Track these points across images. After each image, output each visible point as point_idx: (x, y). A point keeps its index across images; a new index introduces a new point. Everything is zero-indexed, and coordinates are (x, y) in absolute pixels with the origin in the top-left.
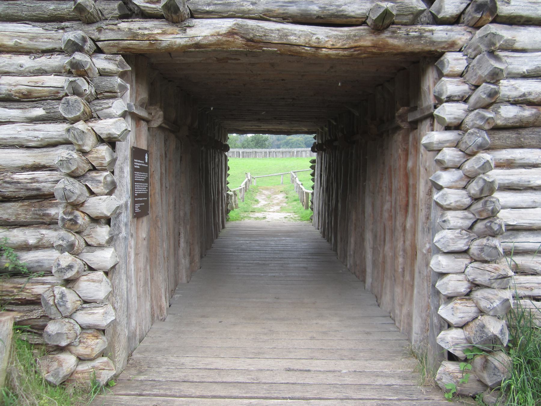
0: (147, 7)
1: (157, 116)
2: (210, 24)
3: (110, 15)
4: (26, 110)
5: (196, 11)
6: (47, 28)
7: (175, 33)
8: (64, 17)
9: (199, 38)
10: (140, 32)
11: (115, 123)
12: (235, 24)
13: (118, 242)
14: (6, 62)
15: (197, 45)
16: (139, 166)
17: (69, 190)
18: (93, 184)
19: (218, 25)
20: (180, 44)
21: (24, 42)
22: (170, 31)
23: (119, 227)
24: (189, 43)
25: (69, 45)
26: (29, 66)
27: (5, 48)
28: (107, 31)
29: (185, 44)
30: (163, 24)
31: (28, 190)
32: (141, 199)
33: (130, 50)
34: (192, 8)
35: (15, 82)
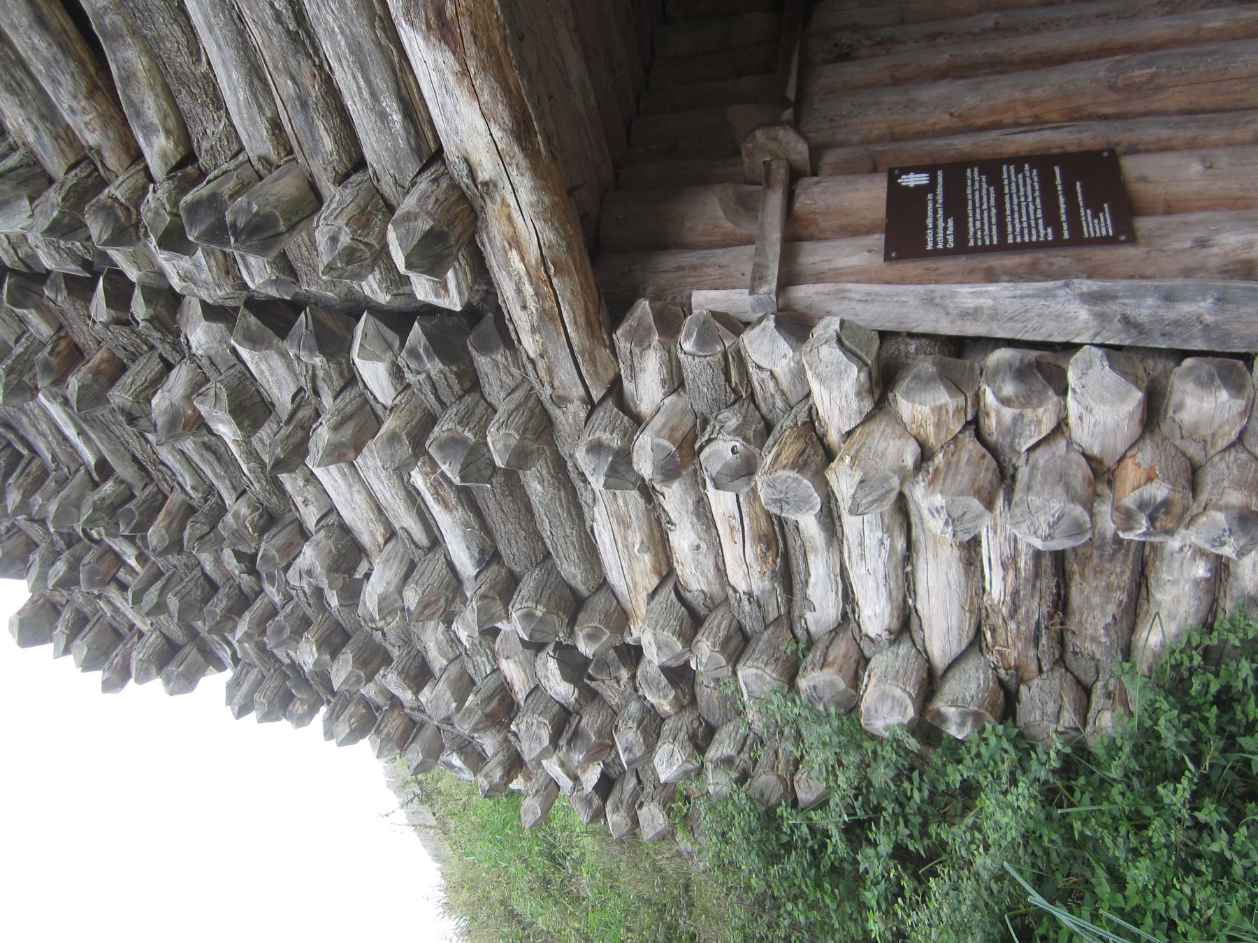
0: (458, 286)
1: (772, 145)
2: (442, 107)
3: (515, 371)
4: (807, 544)
5: (418, 151)
6: (590, 501)
7: (506, 210)
8: (552, 462)
9: (498, 134)
10: (532, 305)
11: (822, 381)
12: (412, 24)
13: (1237, 325)
14: (694, 571)
15: (522, 132)
16: (945, 221)
17: (1051, 526)
18: (1027, 433)
19: (435, 79)
20: (534, 189)
21: (637, 537)
22: (505, 227)
23: (1176, 323)
24: (524, 163)
25: (618, 482)
26: (692, 532)
27: (660, 565)
28: (556, 383)
29: (528, 174)
30: (492, 247)
31: (1037, 575)
32: (1062, 200)
33: (593, 318)
34: (412, 167)
35: (740, 566)
